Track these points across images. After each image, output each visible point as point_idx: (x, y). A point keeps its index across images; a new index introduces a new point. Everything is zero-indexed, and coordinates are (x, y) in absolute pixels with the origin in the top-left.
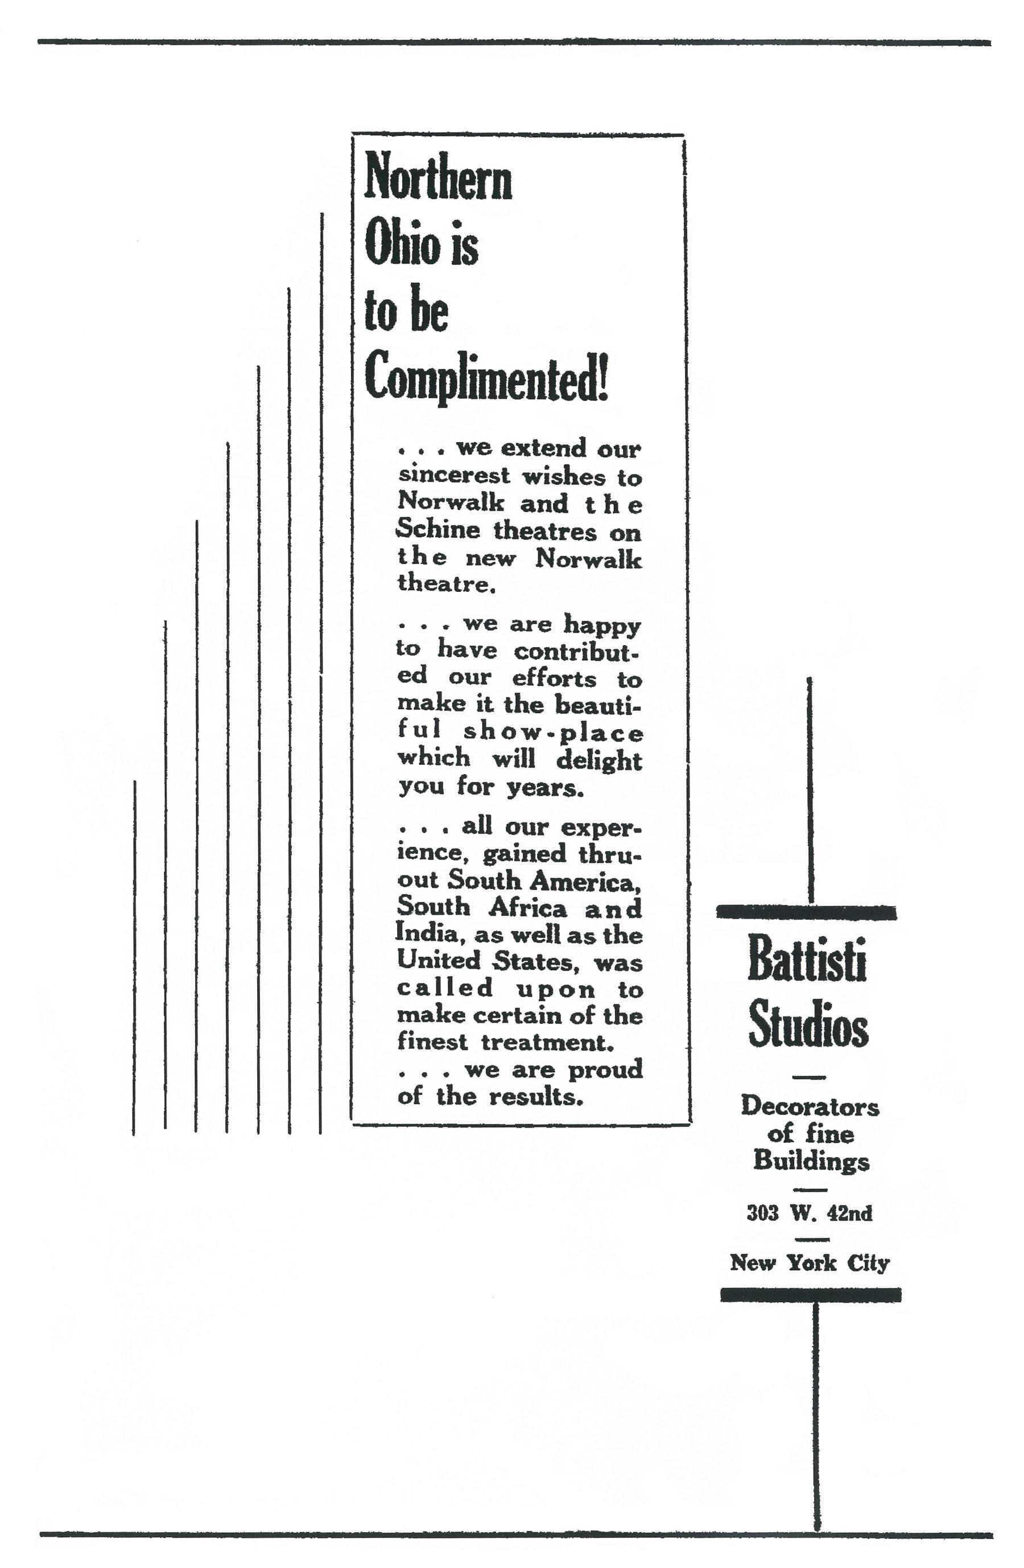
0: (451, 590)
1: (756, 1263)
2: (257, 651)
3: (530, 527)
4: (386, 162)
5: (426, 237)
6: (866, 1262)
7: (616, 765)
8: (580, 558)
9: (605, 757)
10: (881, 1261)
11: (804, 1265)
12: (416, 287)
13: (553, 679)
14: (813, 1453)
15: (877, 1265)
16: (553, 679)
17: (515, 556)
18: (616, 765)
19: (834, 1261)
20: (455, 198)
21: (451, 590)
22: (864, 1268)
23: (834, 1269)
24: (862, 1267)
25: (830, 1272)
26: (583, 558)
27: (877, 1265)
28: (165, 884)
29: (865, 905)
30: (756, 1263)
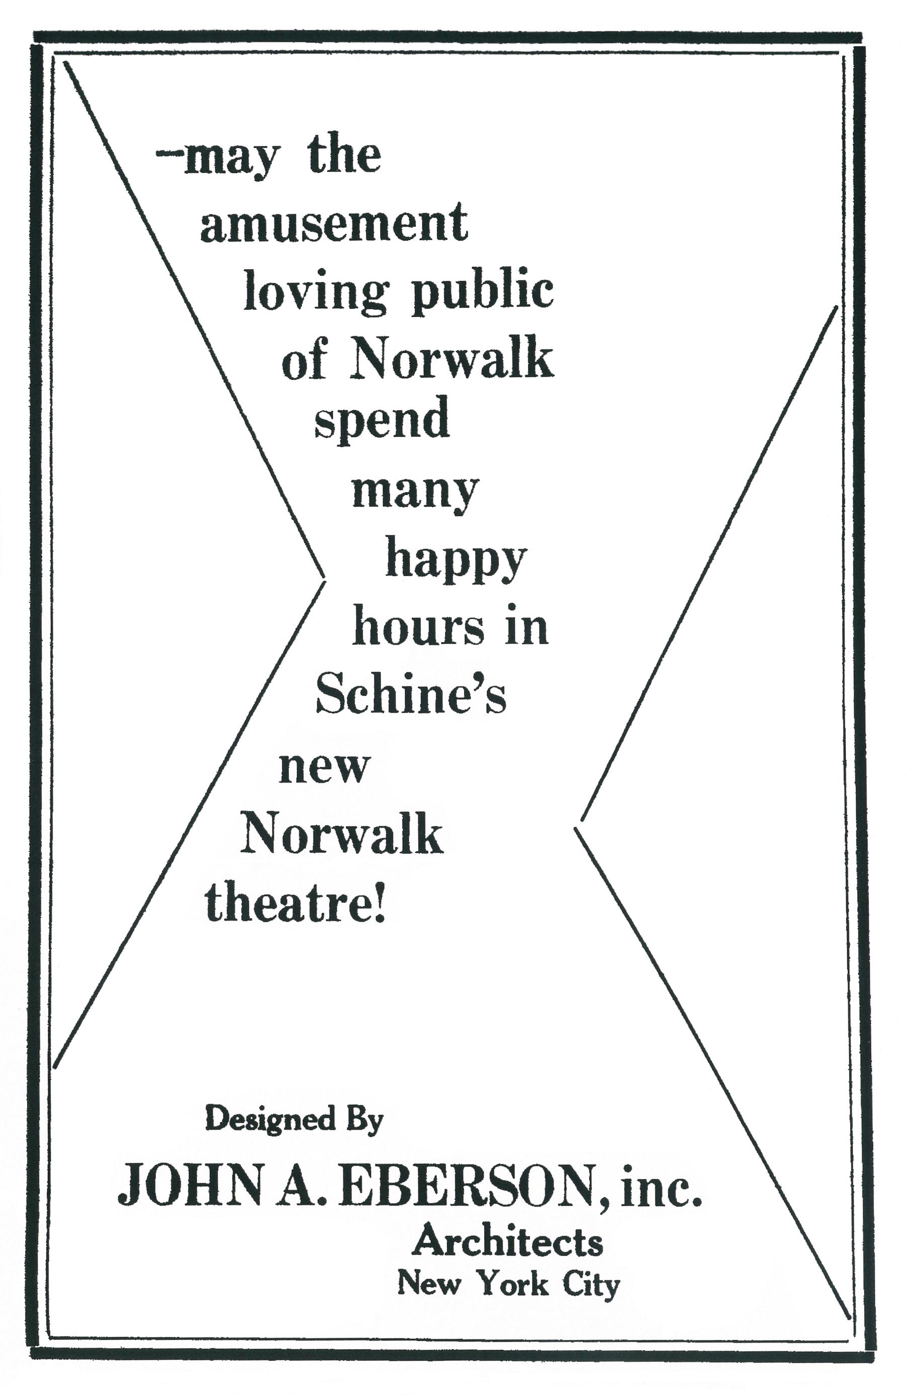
0: (211, 172)
1: (433, 1285)
2: (842, 623)
3: (240, 1115)
4: (417, 1276)
5: (394, 368)
6: (588, 1283)
7: (282, 1125)
8: (437, 354)
9: (603, 1253)
10: (608, 1283)
11: (503, 1287)
12: (451, 1205)
13: (325, 1119)
14: (400, 630)
15: (603, 1287)
16: (325, 1119)
17: (413, 1253)
18: (282, 1125)
19: (544, 1282)
20: (298, 1166)
21: (211, 172)
22: (584, 1292)
23: (544, 1293)
24: (582, 1291)
25: (540, 1297)
26: (442, 354)
27: (603, 1287)
28: (222, 373)
29: (860, 1066)
30: (433, 1285)
